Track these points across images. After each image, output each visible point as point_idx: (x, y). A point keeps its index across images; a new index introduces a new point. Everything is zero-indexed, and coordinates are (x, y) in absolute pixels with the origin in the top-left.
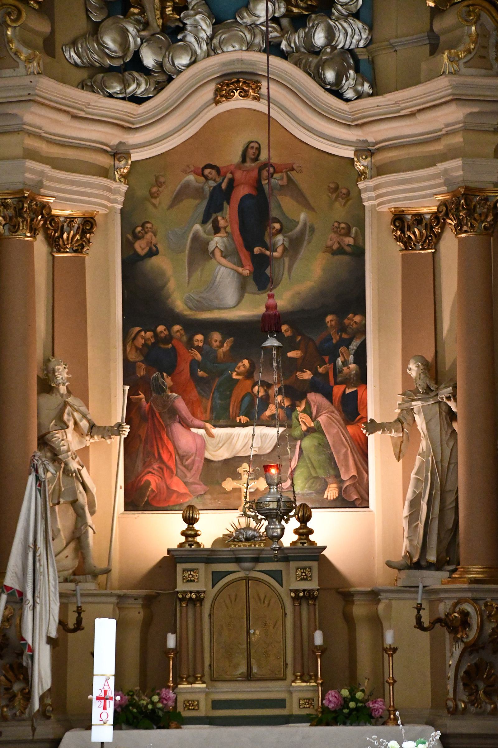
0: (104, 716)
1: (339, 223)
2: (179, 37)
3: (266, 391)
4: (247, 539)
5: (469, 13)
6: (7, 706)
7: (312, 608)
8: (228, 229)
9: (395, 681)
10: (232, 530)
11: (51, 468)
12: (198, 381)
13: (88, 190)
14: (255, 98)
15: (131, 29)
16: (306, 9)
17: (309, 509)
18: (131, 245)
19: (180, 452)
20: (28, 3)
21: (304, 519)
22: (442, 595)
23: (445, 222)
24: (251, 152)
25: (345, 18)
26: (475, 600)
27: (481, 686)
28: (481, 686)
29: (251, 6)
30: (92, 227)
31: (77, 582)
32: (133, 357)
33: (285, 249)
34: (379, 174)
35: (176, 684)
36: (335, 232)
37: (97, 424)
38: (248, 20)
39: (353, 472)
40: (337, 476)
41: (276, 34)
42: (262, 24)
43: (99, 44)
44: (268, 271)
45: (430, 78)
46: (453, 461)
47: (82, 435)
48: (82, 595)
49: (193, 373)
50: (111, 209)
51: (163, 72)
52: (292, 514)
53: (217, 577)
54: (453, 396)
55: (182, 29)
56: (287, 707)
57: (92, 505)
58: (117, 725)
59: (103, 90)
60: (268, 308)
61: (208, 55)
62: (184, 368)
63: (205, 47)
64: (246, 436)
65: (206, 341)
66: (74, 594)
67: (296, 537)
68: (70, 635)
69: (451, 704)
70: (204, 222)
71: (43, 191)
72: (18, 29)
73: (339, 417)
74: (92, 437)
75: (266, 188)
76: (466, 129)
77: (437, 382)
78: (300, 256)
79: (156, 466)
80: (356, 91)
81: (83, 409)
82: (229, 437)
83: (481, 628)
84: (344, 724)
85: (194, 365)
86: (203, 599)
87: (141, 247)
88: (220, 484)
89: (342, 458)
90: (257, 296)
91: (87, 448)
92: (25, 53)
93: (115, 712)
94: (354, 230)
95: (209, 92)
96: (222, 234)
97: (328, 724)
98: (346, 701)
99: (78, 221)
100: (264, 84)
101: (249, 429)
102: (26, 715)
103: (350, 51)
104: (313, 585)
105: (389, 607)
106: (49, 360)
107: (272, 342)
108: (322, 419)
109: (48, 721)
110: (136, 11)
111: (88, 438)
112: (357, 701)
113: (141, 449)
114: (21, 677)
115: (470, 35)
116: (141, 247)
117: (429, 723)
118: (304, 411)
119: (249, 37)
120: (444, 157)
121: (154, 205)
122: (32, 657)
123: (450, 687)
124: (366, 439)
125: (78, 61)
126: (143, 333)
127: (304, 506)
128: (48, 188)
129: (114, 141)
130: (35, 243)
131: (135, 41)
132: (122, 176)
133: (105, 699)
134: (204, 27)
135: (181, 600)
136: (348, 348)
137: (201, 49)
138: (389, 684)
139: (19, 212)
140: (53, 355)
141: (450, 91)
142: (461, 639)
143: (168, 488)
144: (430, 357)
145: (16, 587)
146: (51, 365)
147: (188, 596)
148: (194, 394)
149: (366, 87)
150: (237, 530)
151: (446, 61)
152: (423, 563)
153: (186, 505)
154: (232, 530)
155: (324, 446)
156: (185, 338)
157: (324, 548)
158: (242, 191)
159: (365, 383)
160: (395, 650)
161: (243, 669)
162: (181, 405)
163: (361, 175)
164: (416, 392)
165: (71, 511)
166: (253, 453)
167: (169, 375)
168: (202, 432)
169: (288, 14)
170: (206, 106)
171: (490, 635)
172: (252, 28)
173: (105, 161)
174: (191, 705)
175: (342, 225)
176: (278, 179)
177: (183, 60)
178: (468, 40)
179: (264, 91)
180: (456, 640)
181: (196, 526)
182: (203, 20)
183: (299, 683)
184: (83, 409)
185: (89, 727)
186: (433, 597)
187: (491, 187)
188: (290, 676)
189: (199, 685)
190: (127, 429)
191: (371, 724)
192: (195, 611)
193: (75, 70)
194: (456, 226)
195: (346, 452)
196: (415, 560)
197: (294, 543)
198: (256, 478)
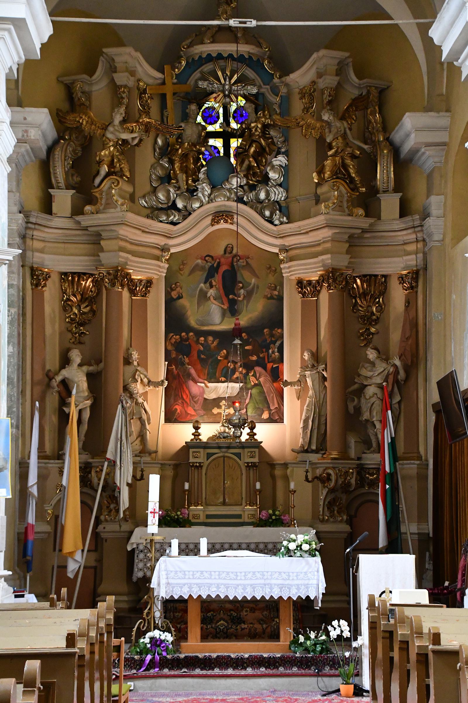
0: (154, 521)
1: (271, 284)
2: (195, 194)
3: (234, 366)
4: (224, 438)
5: (334, 186)
6: (107, 515)
7: (255, 471)
8: (217, 286)
9: (294, 506)
10: (217, 433)
11: (129, 402)
12: (202, 361)
13: (140, 265)
14: (231, 223)
15: (172, 190)
16: (256, 182)
17: (255, 423)
18: (170, 294)
19: (192, 395)
20: (123, 178)
21: (252, 428)
22: (319, 466)
23: (322, 285)
24: (228, 249)
25: (275, 186)
26: (334, 468)
27: (336, 509)
28: (336, 509)
29: (230, 180)
30: (151, 285)
31: (141, 457)
32: (169, 348)
33: (244, 297)
34: (291, 261)
35: (189, 507)
36: (269, 289)
37: (152, 380)
38: (228, 186)
39: (277, 406)
40: (269, 407)
41: (241, 193)
42: (234, 188)
43: (156, 197)
44: (236, 307)
45: (315, 216)
46: (325, 401)
47: (144, 385)
48: (144, 463)
49: (199, 356)
50: (161, 276)
51: (187, 210)
52: (246, 425)
53: (209, 455)
54: (325, 369)
55: (197, 190)
56: (243, 518)
57: (149, 420)
58: (160, 525)
59: (157, 219)
60: (235, 325)
61: (209, 203)
62: (195, 354)
63: (207, 199)
64: (224, 387)
65: (206, 340)
66: (139, 462)
67: (248, 437)
68: (138, 482)
69: (321, 517)
70: (205, 283)
71: (127, 267)
72: (117, 190)
73: (270, 379)
74: (149, 387)
75: (236, 267)
76: (333, 240)
77: (318, 362)
78: (253, 298)
79: (180, 401)
80: (280, 221)
81: (145, 373)
82: (216, 388)
83: (336, 481)
84: (270, 526)
85: (199, 352)
86: (202, 466)
87: (174, 294)
88: (211, 411)
89: (271, 398)
90: (231, 319)
91: (147, 392)
92: (120, 201)
93: (159, 519)
94: (278, 287)
95: (208, 220)
96: (214, 288)
97: (262, 526)
98: (271, 516)
99: (144, 281)
100: (235, 216)
101: (226, 384)
102: (117, 520)
103: (277, 202)
104: (256, 460)
105: (292, 471)
106: (129, 349)
107: (237, 341)
108: (261, 380)
109: (128, 523)
110: (174, 181)
111: (147, 387)
112: (276, 515)
113: (173, 393)
114: (115, 501)
115: (334, 196)
116: (174, 294)
117: (310, 526)
118: (253, 376)
119: (228, 194)
120: (322, 253)
121: (181, 274)
122: (120, 492)
123: (321, 509)
124: (283, 389)
125: (146, 205)
126: (175, 336)
127: (252, 422)
128: (132, 266)
129: (163, 244)
130: (123, 292)
131: (173, 196)
132: (166, 260)
133: (154, 513)
134: (207, 189)
135: (192, 466)
136: (275, 345)
137: (205, 200)
138: (292, 507)
139: (116, 277)
140: (131, 346)
141: (325, 222)
142: (327, 487)
143: (186, 412)
144: (314, 350)
145: (112, 458)
146: (130, 352)
147: (195, 465)
148: (199, 367)
149: (285, 219)
150: (219, 433)
151: (323, 207)
152: (309, 450)
153: (194, 421)
154: (217, 433)
155: (262, 393)
156: (195, 339)
157: (262, 442)
158: (224, 268)
159: (283, 362)
160: (295, 492)
161: (221, 500)
162: (193, 371)
163: (282, 261)
164: (307, 367)
165: (139, 422)
166: (227, 396)
167: (187, 357)
168: (203, 385)
169: (248, 184)
170: (207, 227)
171: (341, 485)
172: (230, 190)
173: (157, 252)
174: (195, 516)
175: (273, 285)
176: (242, 263)
177: (196, 205)
178: (333, 198)
179: (235, 220)
180: (324, 487)
181: (199, 431)
182: (207, 186)
183: (248, 507)
184: (145, 373)
185: (147, 526)
186: (314, 466)
187: (344, 268)
188: (244, 504)
189: (200, 507)
190: (166, 383)
191: (282, 526)
192: (198, 471)
193: (144, 209)
194: (327, 287)
195: (273, 396)
196: (306, 448)
197: (247, 440)
198: (229, 408)
